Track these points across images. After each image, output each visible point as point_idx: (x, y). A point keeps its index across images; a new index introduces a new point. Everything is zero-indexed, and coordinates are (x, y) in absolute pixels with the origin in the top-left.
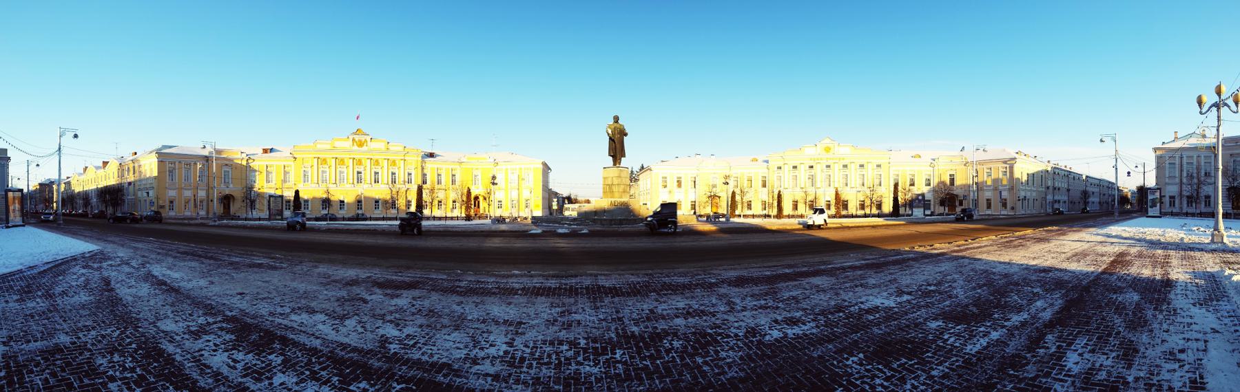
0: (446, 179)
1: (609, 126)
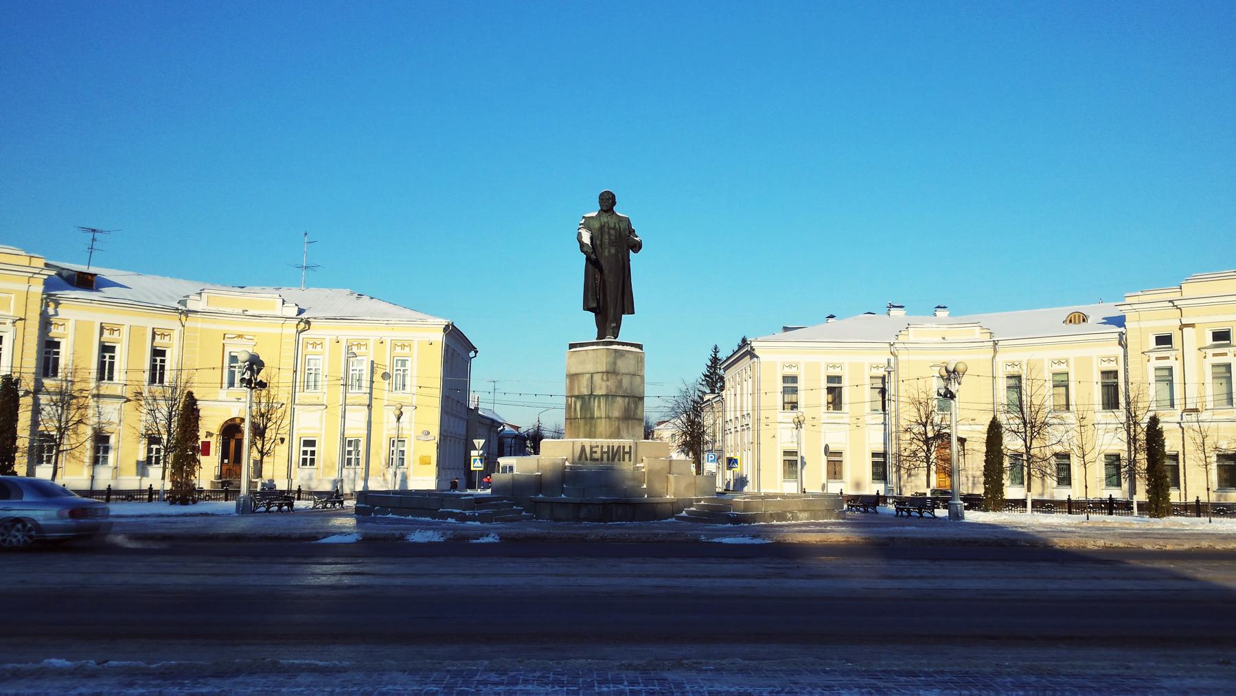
0: (130, 364)
1: (587, 223)
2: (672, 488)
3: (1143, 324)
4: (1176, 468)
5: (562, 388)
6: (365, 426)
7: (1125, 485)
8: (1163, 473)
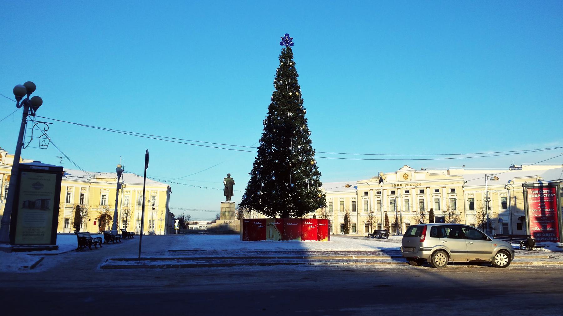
5: (220, 209)
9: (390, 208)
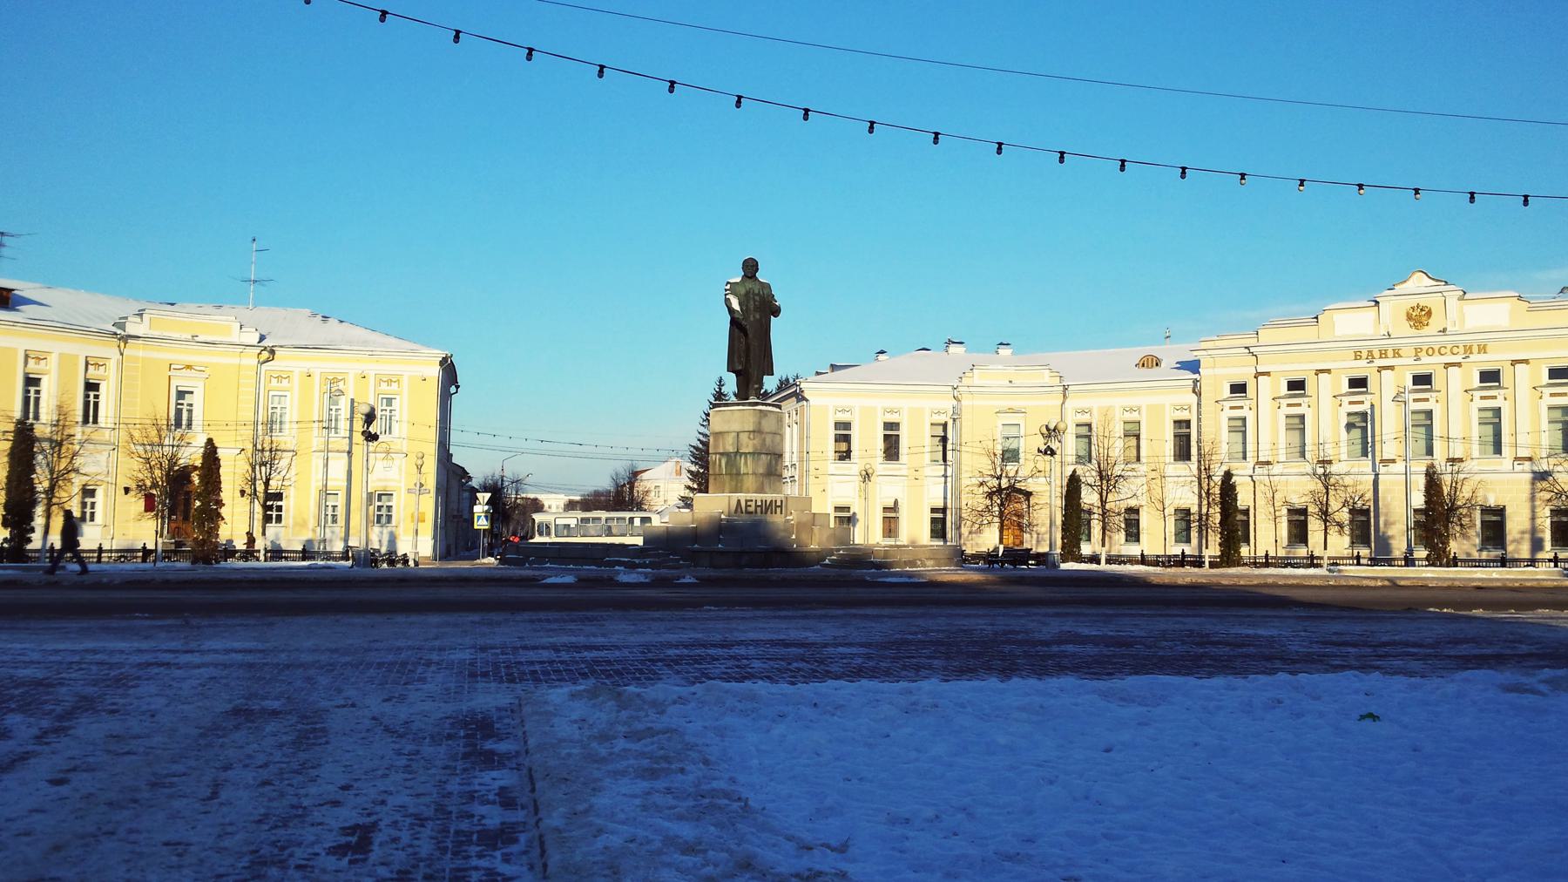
1: (733, 288)
2: (816, 538)
3: (1218, 371)
4: (1247, 523)
6: (345, 476)
7: (1194, 541)
8: (1235, 527)
9: (1344, 449)
